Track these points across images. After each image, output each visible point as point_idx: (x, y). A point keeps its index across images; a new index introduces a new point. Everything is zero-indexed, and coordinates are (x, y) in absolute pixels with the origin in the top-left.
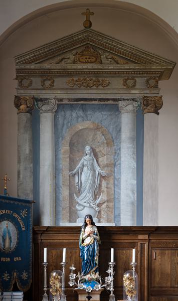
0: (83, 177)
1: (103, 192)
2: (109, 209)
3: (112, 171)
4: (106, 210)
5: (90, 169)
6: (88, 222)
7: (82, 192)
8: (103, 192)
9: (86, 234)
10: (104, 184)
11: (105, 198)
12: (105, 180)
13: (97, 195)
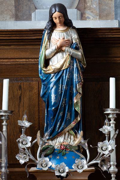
6: (57, 21)
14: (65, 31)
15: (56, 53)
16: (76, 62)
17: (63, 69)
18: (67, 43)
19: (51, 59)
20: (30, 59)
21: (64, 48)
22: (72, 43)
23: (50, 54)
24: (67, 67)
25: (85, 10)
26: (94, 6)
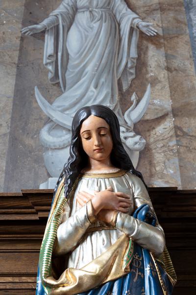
0: (74, 40)
1: (154, 82)
2: (185, 141)
3: (178, 21)
4: (173, 143)
5: (97, 16)
6: (90, 145)
7: (68, 82)
8: (154, 82)
9: (81, 211)
10: (155, 57)
11: (165, 102)
12: (158, 45)
13: (129, 92)
14: (116, 175)
15: (89, 232)
16: (150, 261)
17: (109, 279)
18: (121, 203)
19: (74, 254)
20: (24, 278)
21: (111, 217)
22: (135, 207)
23: (71, 235)
24: (121, 274)
25: (153, 179)
26: (171, 171)
